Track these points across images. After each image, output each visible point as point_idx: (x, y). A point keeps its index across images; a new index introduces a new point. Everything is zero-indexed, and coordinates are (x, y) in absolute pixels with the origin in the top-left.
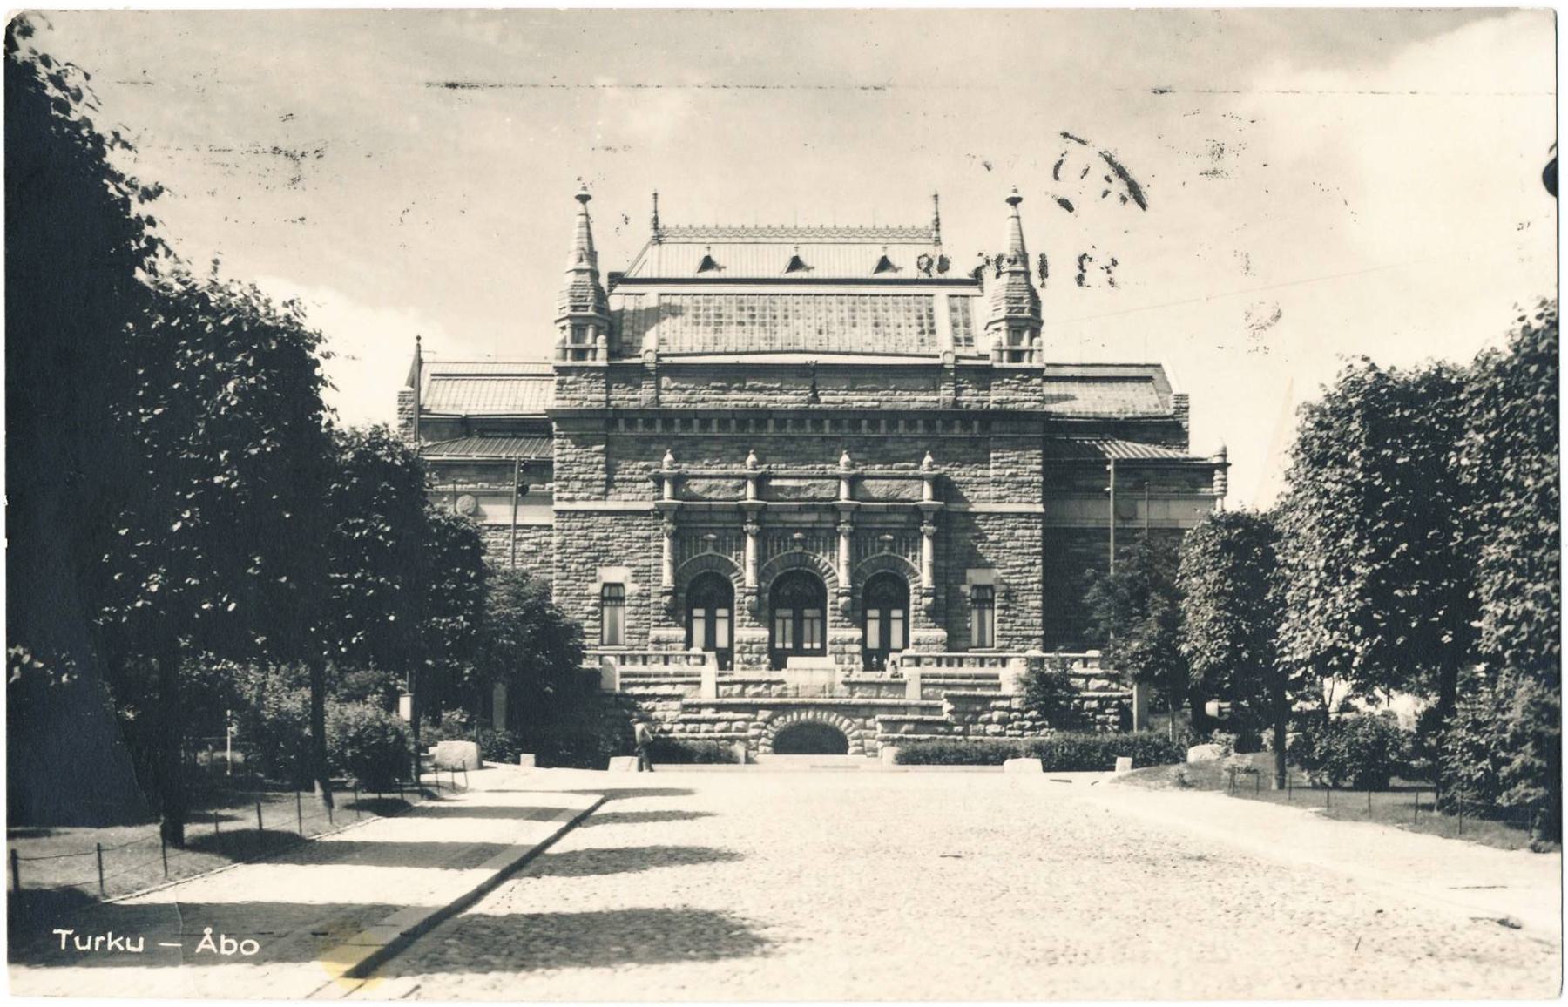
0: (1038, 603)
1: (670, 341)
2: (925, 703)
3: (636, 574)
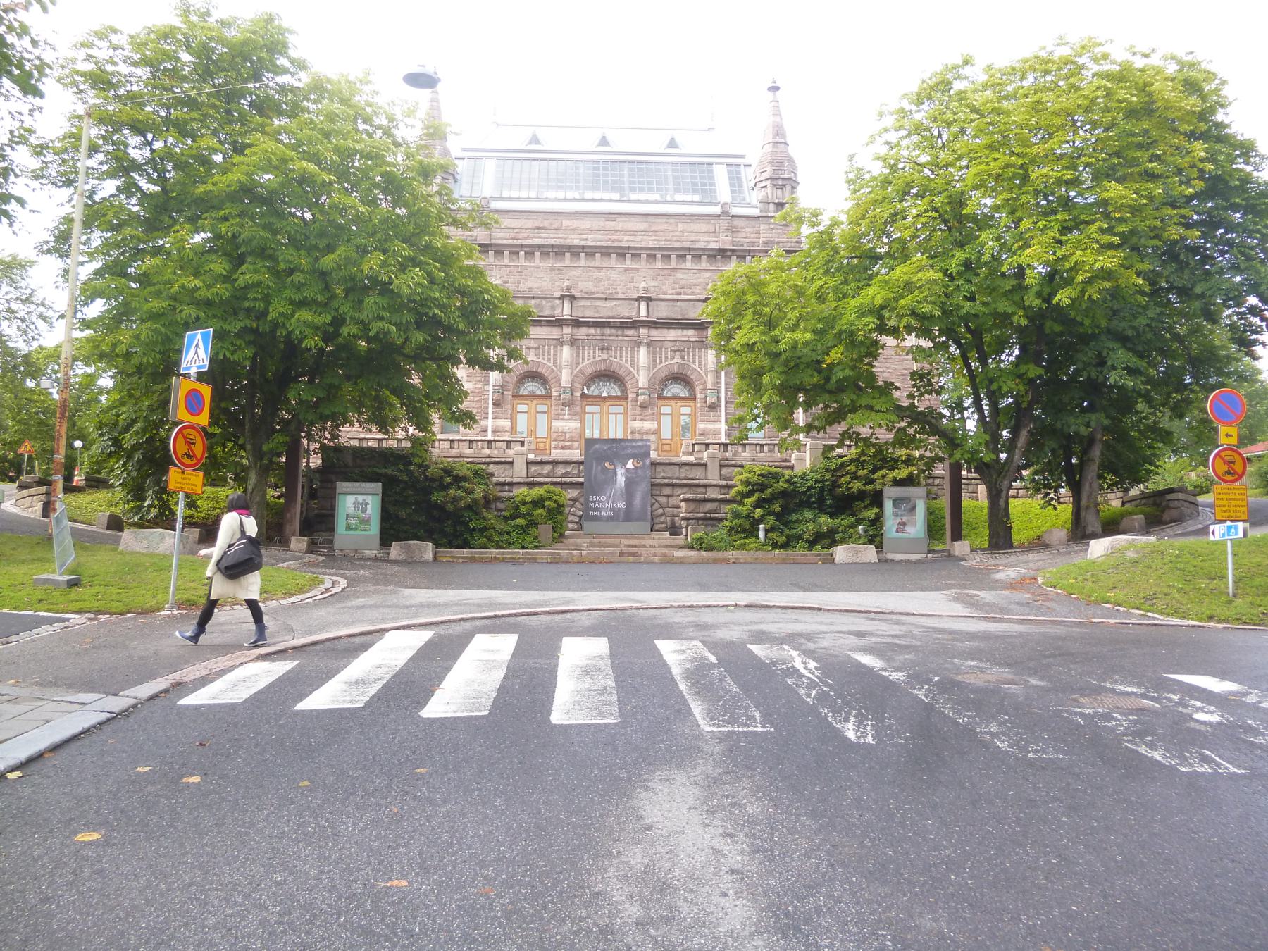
2: (724, 483)
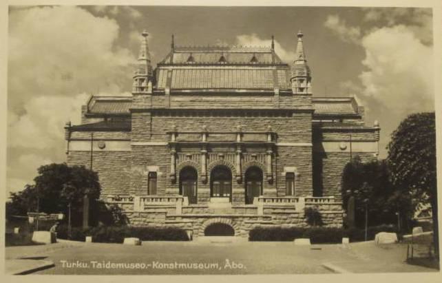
0: (311, 179)
1: (365, 116)
2: (264, 215)
3: (161, 169)
